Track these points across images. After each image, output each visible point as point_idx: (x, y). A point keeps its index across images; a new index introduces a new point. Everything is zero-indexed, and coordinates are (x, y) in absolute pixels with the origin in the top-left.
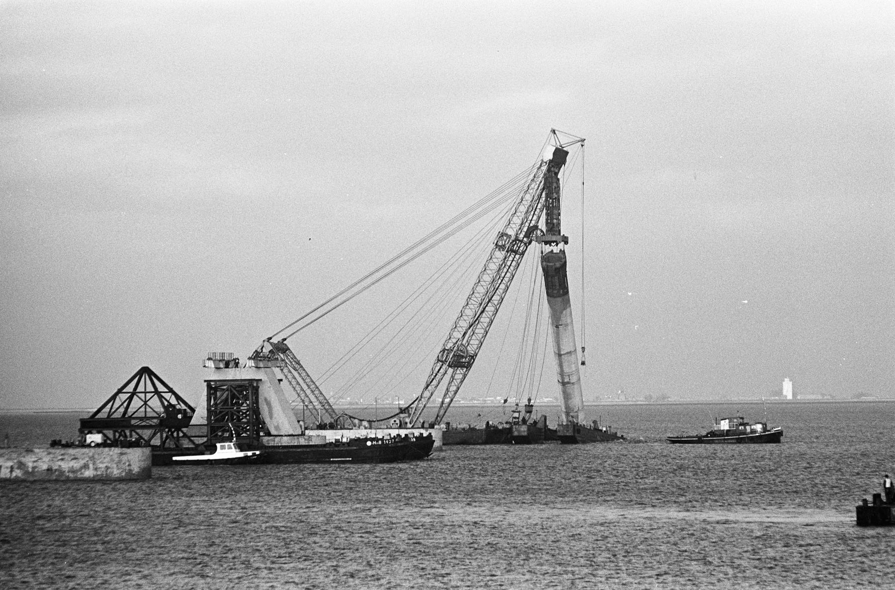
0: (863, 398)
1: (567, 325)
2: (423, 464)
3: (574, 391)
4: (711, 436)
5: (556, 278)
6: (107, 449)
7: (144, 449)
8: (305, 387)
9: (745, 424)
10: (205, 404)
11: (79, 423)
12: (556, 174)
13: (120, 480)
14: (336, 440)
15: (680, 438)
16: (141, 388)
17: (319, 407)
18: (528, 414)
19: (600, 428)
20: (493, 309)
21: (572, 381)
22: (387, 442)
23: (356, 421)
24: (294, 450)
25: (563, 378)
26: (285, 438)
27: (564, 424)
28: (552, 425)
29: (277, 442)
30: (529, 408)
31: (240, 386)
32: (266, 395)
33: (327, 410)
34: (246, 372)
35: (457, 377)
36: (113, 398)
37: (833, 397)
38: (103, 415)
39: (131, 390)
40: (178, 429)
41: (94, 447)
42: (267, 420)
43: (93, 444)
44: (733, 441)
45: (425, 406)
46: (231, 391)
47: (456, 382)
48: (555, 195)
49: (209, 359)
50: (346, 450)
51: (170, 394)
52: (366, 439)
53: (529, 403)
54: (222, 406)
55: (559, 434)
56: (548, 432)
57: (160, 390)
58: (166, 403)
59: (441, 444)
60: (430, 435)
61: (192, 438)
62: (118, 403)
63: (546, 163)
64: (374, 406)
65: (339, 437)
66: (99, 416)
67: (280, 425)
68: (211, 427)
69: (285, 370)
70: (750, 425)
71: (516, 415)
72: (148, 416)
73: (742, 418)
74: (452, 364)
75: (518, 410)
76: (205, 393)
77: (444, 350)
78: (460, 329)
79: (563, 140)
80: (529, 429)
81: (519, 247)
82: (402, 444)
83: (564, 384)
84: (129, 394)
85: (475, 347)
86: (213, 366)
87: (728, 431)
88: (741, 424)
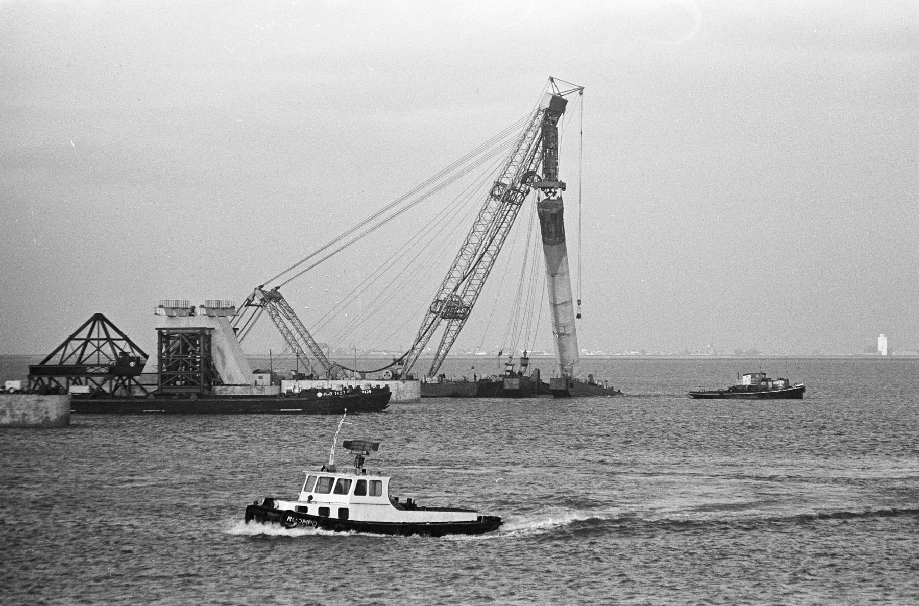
1: (563, 274)
2: (381, 416)
3: (569, 343)
4: (733, 392)
6: (24, 396)
10: (156, 352)
11: (28, 370)
12: (555, 123)
13: (37, 427)
15: (702, 393)
16: (94, 335)
17: (311, 356)
18: (524, 367)
19: (596, 383)
20: (489, 259)
23: (348, 372)
24: (244, 400)
25: (558, 329)
28: (545, 379)
29: (229, 391)
30: (525, 361)
31: (193, 335)
32: (220, 345)
33: (320, 360)
34: (200, 321)
36: (66, 344)
38: (55, 361)
39: (85, 337)
40: (130, 377)
41: (13, 393)
42: (220, 369)
43: (12, 391)
44: (755, 397)
45: (416, 358)
46: (183, 340)
48: (552, 145)
49: (161, 306)
50: (296, 401)
52: (317, 391)
53: (525, 356)
55: (552, 388)
56: (541, 386)
57: (112, 337)
58: (118, 351)
60: (387, 387)
61: (145, 387)
62: (69, 351)
65: (291, 388)
66: (50, 362)
67: (233, 374)
68: (162, 376)
69: (277, 319)
70: (773, 381)
72: (100, 363)
73: (764, 374)
74: (445, 315)
75: (512, 363)
77: (437, 301)
78: (453, 280)
79: (562, 88)
83: (560, 335)
86: (164, 314)
88: (764, 380)
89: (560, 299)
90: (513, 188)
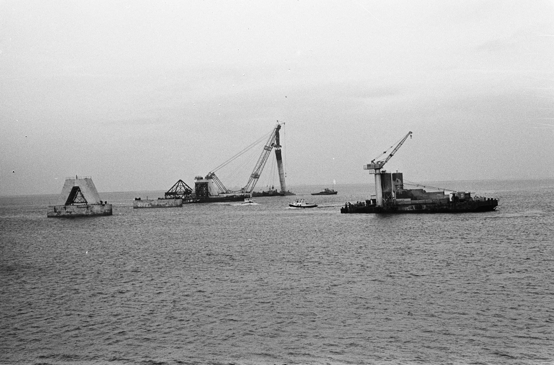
16: (179, 185)
28: (278, 192)
29: (212, 197)
34: (204, 181)
36: (173, 187)
38: (170, 191)
40: (189, 195)
47: (255, 182)
66: (169, 192)
79: (280, 123)
89: (281, 173)
90: (269, 147)
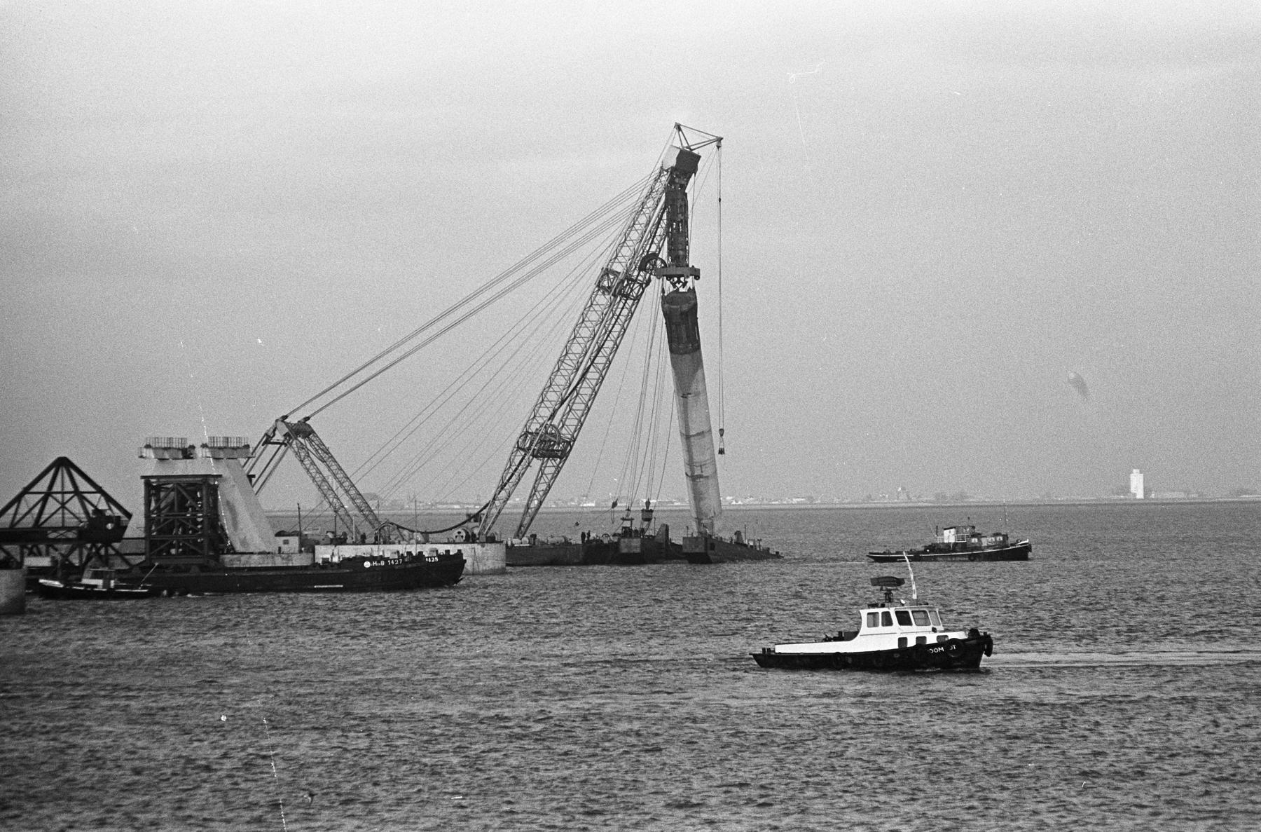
0: (1245, 497)
1: (697, 394)
3: (707, 488)
5: (683, 327)
7: (15, 572)
8: (335, 485)
9: (978, 535)
12: (684, 187)
14: (323, 559)
16: (57, 488)
18: (646, 523)
19: (746, 542)
21: (704, 474)
22: (393, 562)
25: (692, 470)
26: (256, 557)
27: (695, 535)
28: (677, 538)
29: (244, 562)
30: (648, 514)
31: (190, 484)
34: (201, 465)
35: (547, 471)
36: (18, 499)
37: (1200, 495)
39: (45, 489)
40: (107, 544)
45: (499, 513)
46: (179, 493)
47: (545, 479)
48: (680, 217)
49: (148, 446)
51: (98, 495)
52: (364, 559)
54: (168, 512)
55: (685, 550)
58: (90, 509)
59: (504, 565)
60: (460, 553)
61: (127, 557)
63: (667, 171)
64: (413, 512)
65: (328, 556)
69: (307, 462)
71: (627, 524)
72: (67, 525)
74: (538, 452)
75: (630, 517)
76: (142, 493)
77: (526, 434)
79: (693, 139)
80: (642, 544)
81: (632, 290)
82: (415, 565)
83: (694, 478)
84: (43, 495)
85: (572, 429)
87: (955, 544)
88: (973, 536)
90: (628, 277)
